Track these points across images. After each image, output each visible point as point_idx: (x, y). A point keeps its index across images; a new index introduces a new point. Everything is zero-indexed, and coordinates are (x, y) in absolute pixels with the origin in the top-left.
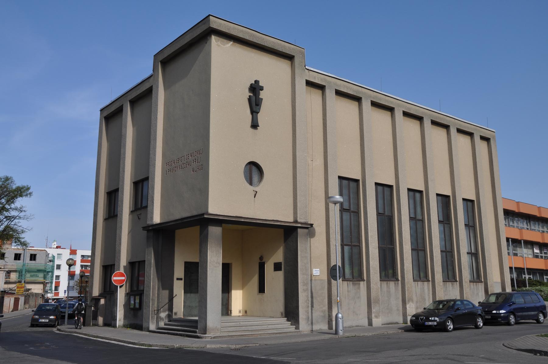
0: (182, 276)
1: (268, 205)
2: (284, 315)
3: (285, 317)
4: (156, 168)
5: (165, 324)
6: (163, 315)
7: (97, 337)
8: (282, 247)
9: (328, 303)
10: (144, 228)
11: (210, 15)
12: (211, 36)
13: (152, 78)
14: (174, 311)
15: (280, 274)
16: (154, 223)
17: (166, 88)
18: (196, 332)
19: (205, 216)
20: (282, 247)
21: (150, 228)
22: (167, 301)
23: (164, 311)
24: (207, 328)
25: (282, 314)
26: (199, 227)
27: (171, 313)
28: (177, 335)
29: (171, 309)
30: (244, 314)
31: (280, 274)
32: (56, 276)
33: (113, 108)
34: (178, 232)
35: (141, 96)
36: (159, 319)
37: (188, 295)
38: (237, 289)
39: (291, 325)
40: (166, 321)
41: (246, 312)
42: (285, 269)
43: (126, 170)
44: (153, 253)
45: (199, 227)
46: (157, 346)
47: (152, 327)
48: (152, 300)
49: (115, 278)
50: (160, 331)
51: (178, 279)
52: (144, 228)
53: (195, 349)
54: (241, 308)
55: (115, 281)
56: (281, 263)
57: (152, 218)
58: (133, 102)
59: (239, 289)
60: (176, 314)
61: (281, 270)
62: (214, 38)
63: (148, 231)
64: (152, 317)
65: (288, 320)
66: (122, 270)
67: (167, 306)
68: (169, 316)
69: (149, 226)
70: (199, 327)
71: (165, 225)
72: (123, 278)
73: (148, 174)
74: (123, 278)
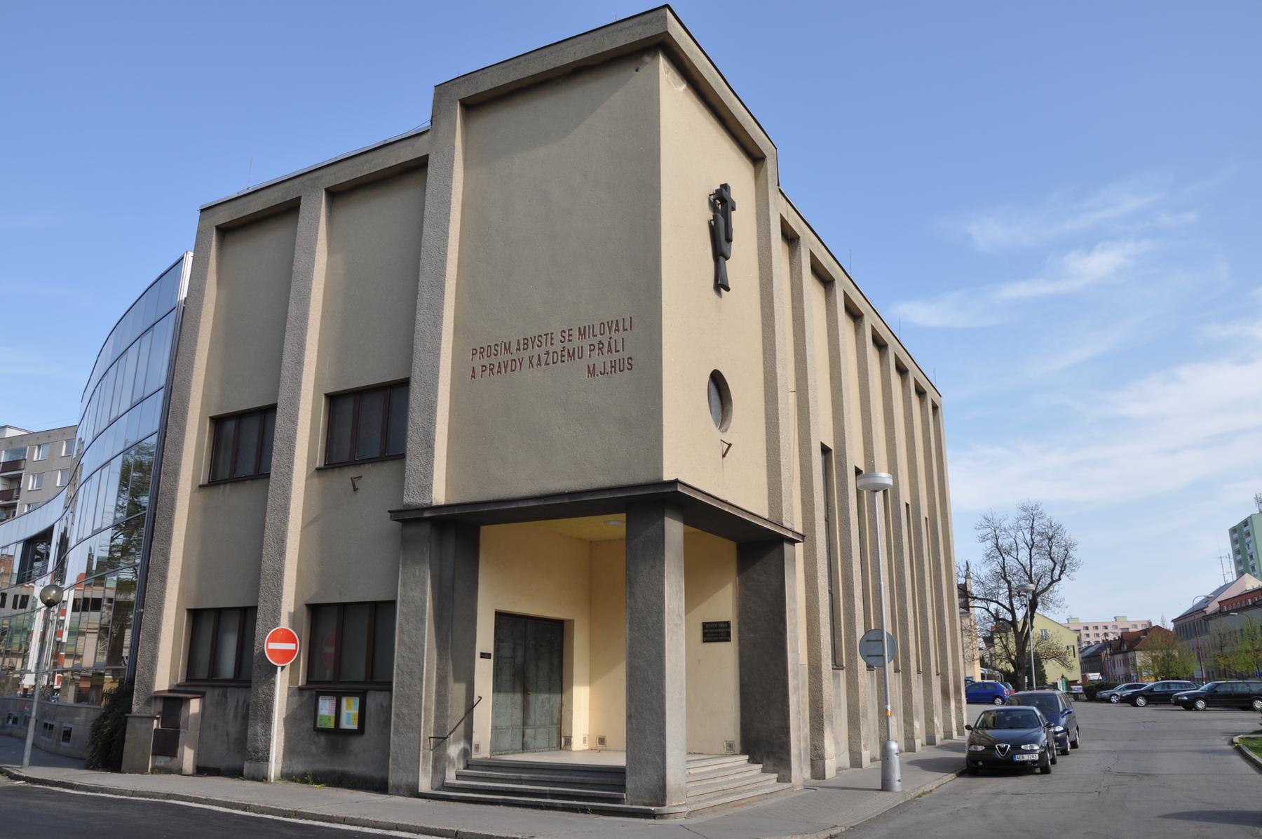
0: (491, 650)
1: (739, 486)
3: (743, 752)
4: (442, 358)
5: (458, 777)
6: (454, 750)
7: (397, 828)
10: (395, 514)
11: (667, 6)
12: (656, 55)
13: (425, 137)
14: (475, 740)
15: (727, 654)
16: (434, 504)
17: (466, 168)
18: (619, 800)
19: (680, 489)
21: (427, 514)
22: (461, 713)
23: (456, 741)
25: (730, 746)
26: (623, 516)
28: (584, 810)
29: (468, 736)
30: (595, 744)
31: (727, 654)
33: (276, 198)
34: (489, 534)
35: (386, 178)
36: (440, 762)
38: (580, 684)
39: (764, 771)
40: (460, 766)
41: (602, 741)
42: (740, 639)
43: (306, 360)
44: (429, 582)
45: (623, 516)
47: (425, 785)
49: (273, 646)
51: (484, 655)
52: (395, 514)
55: (272, 652)
56: (728, 623)
57: (427, 488)
58: (335, 194)
60: (477, 747)
61: (729, 640)
62: (663, 63)
63: (404, 522)
65: (753, 760)
66: (284, 623)
67: (461, 728)
68: (466, 753)
69: (409, 509)
70: (628, 786)
72: (291, 646)
73: (277, 395)
74: (291, 646)
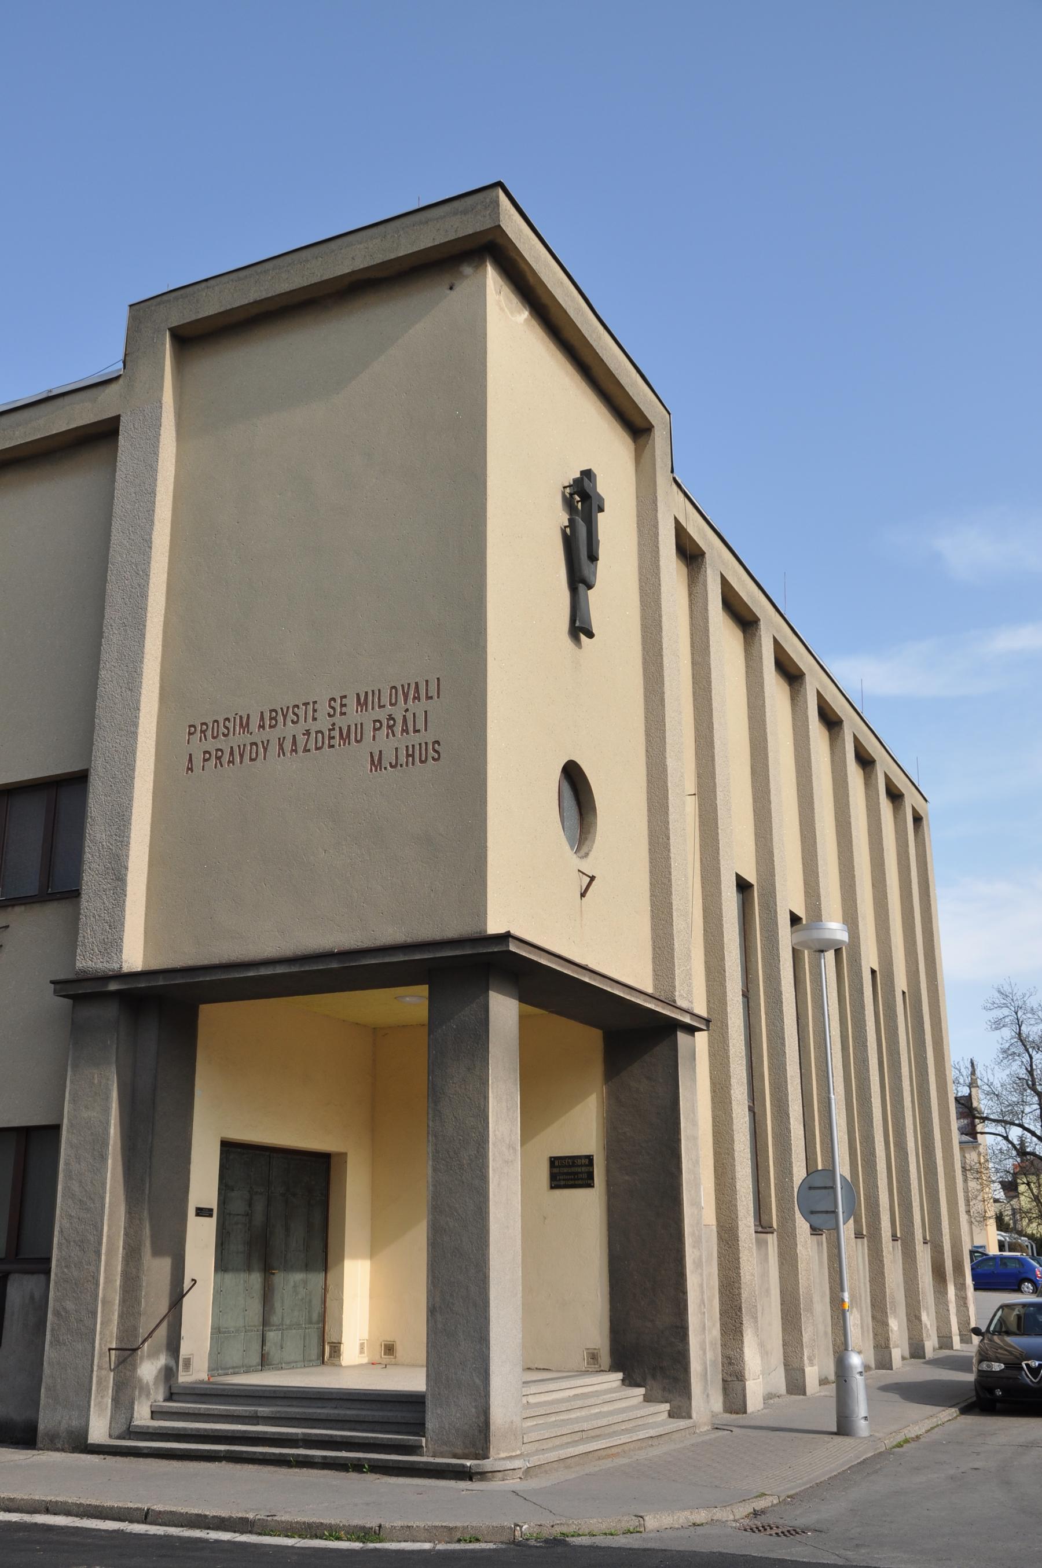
2: (605, 1359)
3: (614, 1368)
5: (154, 1414)
6: (149, 1370)
8: (966, 1122)
9: (723, 1313)
10: (61, 987)
16: (126, 969)
20: (966, 1122)
21: (113, 987)
22: (163, 1307)
23: (153, 1355)
24: (492, 1428)
25: (594, 1357)
27: (172, 1363)
28: (357, 1467)
29: (173, 1346)
30: (378, 1355)
32: (1001, 1250)
34: (210, 1015)
37: (229, 1277)
38: (355, 1257)
39: (647, 1399)
40: (158, 1396)
41: (389, 1349)
46: (408, 1533)
47: (99, 1431)
48: (104, 1302)
50: (131, 1446)
52: (61, 987)
53: (601, 1541)
54: (366, 1336)
56: (590, 1159)
57: (114, 944)
59: (362, 1257)
60: (188, 1363)
61: (590, 1185)
63: (76, 998)
64: (99, 1383)
65: (629, 1381)
67: (162, 1332)
68: (169, 1374)
70: (429, 1425)
71: (161, 982)
